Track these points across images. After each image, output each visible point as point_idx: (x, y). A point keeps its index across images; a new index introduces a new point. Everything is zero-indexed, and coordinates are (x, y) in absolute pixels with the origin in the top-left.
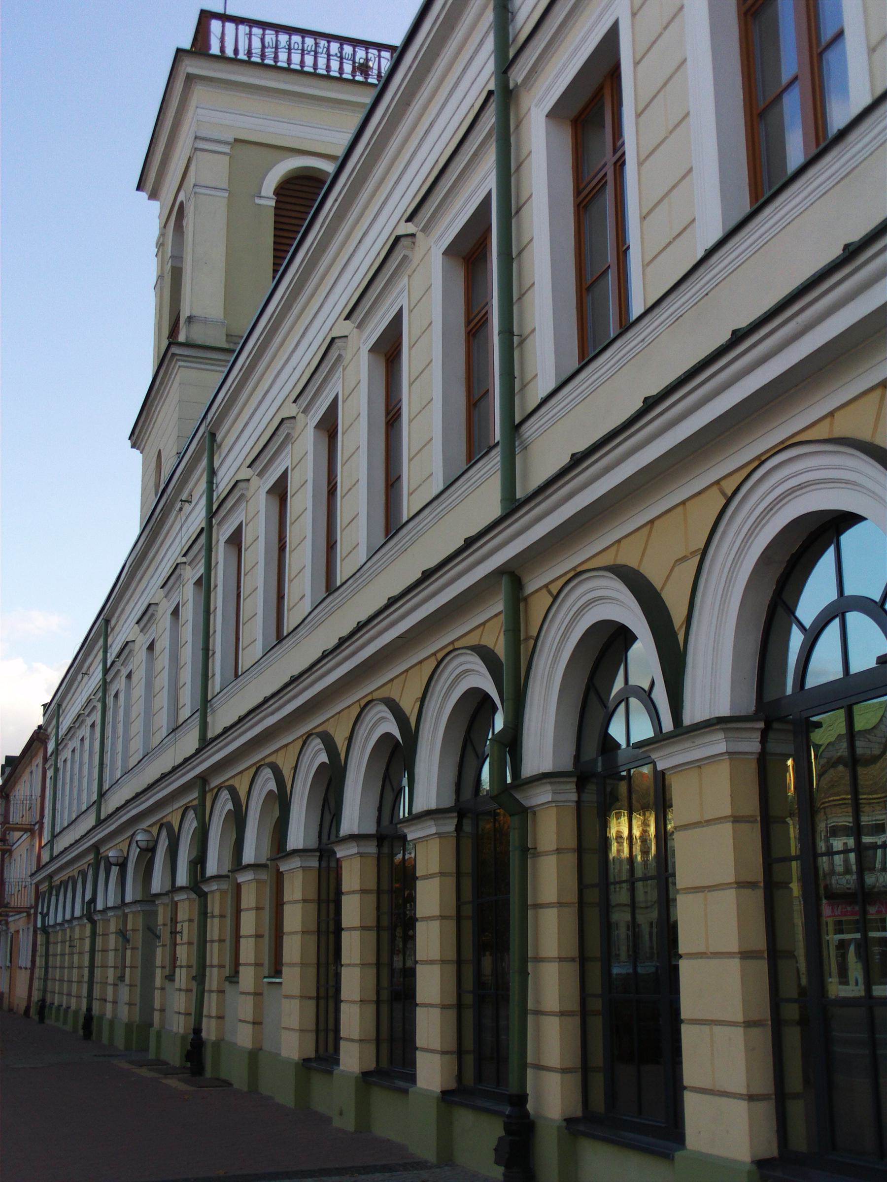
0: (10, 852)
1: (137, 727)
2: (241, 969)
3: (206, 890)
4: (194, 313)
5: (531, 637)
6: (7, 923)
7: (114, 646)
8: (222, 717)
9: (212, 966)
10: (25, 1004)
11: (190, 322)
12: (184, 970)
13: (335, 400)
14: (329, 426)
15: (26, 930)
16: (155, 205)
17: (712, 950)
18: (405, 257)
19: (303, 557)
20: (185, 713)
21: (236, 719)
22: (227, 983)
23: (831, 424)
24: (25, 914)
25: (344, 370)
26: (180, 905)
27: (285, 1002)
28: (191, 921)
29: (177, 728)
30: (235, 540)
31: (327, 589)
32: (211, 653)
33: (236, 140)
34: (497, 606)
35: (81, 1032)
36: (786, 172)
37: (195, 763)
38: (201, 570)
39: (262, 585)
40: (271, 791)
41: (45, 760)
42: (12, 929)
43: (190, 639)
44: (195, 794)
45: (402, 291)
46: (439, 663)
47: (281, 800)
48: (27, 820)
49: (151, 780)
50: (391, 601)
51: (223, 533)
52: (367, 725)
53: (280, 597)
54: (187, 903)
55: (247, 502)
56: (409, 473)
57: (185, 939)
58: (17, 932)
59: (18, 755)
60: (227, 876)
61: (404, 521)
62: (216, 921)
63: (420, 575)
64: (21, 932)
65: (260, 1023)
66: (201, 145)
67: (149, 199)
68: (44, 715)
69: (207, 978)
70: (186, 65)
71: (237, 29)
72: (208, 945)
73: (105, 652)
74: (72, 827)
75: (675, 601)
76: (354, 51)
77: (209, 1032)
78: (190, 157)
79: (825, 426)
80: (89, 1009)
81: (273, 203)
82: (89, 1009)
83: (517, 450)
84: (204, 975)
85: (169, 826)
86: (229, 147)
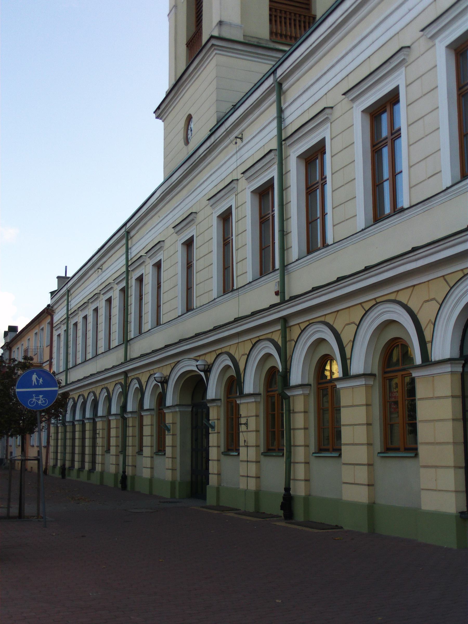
2: (144, 448)
3: (126, 416)
5: (293, 340)
8: (139, 347)
9: (129, 446)
12: (100, 448)
20: (114, 343)
22: (262, 456)
23: (397, 295)
26: (112, 422)
27: (111, 457)
28: (103, 429)
30: (140, 279)
31: (140, 333)
35: (120, 486)
38: (65, 328)
40: (137, 388)
43: (150, 291)
45: (161, 254)
47: (109, 399)
51: (135, 275)
52: (309, 333)
54: (101, 422)
55: (331, 123)
56: (238, 269)
57: (101, 436)
62: (131, 429)
65: (153, 468)
75: (346, 337)
77: (129, 471)
79: (394, 295)
80: (124, 472)
82: (124, 472)
84: (126, 450)
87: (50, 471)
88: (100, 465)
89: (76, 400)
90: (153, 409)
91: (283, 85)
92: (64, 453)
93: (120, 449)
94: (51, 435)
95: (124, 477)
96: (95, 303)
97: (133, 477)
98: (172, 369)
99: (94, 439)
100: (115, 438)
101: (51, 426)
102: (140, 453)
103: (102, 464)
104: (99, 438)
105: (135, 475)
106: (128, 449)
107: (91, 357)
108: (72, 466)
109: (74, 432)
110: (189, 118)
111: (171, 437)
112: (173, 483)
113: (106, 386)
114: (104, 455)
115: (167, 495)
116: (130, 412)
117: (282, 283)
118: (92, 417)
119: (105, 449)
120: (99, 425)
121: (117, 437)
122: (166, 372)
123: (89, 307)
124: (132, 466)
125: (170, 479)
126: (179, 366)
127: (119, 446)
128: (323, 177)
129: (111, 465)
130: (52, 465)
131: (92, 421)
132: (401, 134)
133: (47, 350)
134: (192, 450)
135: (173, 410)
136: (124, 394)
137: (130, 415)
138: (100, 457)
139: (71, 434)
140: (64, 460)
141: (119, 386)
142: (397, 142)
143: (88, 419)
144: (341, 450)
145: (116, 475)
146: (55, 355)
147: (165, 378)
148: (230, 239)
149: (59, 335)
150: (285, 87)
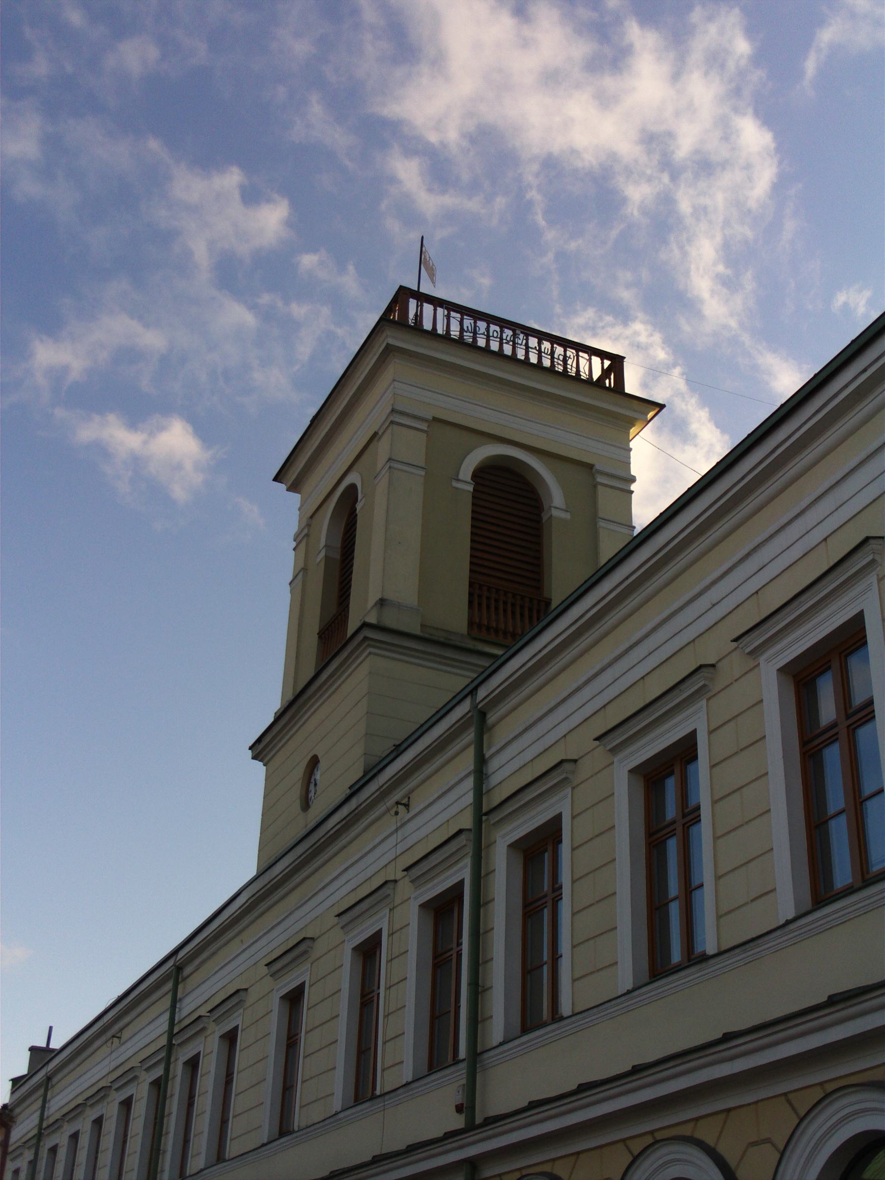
4: (385, 597)
7: (52, 1102)
11: (382, 605)
16: (295, 498)
33: (435, 419)
36: (819, 725)
37: (432, 1152)
51: (184, 1055)
63: (526, 1104)
66: (398, 419)
67: (287, 490)
70: (387, 336)
71: (435, 310)
76: (552, 347)
78: (376, 434)
81: (470, 488)
86: (426, 425)
91: (488, 716)
98: (635, 1159)
110: (314, 762)
117: (471, 1088)
123: (109, 1099)
128: (556, 886)
132: (874, 711)
142: (694, 830)
148: (375, 994)
150: (491, 719)
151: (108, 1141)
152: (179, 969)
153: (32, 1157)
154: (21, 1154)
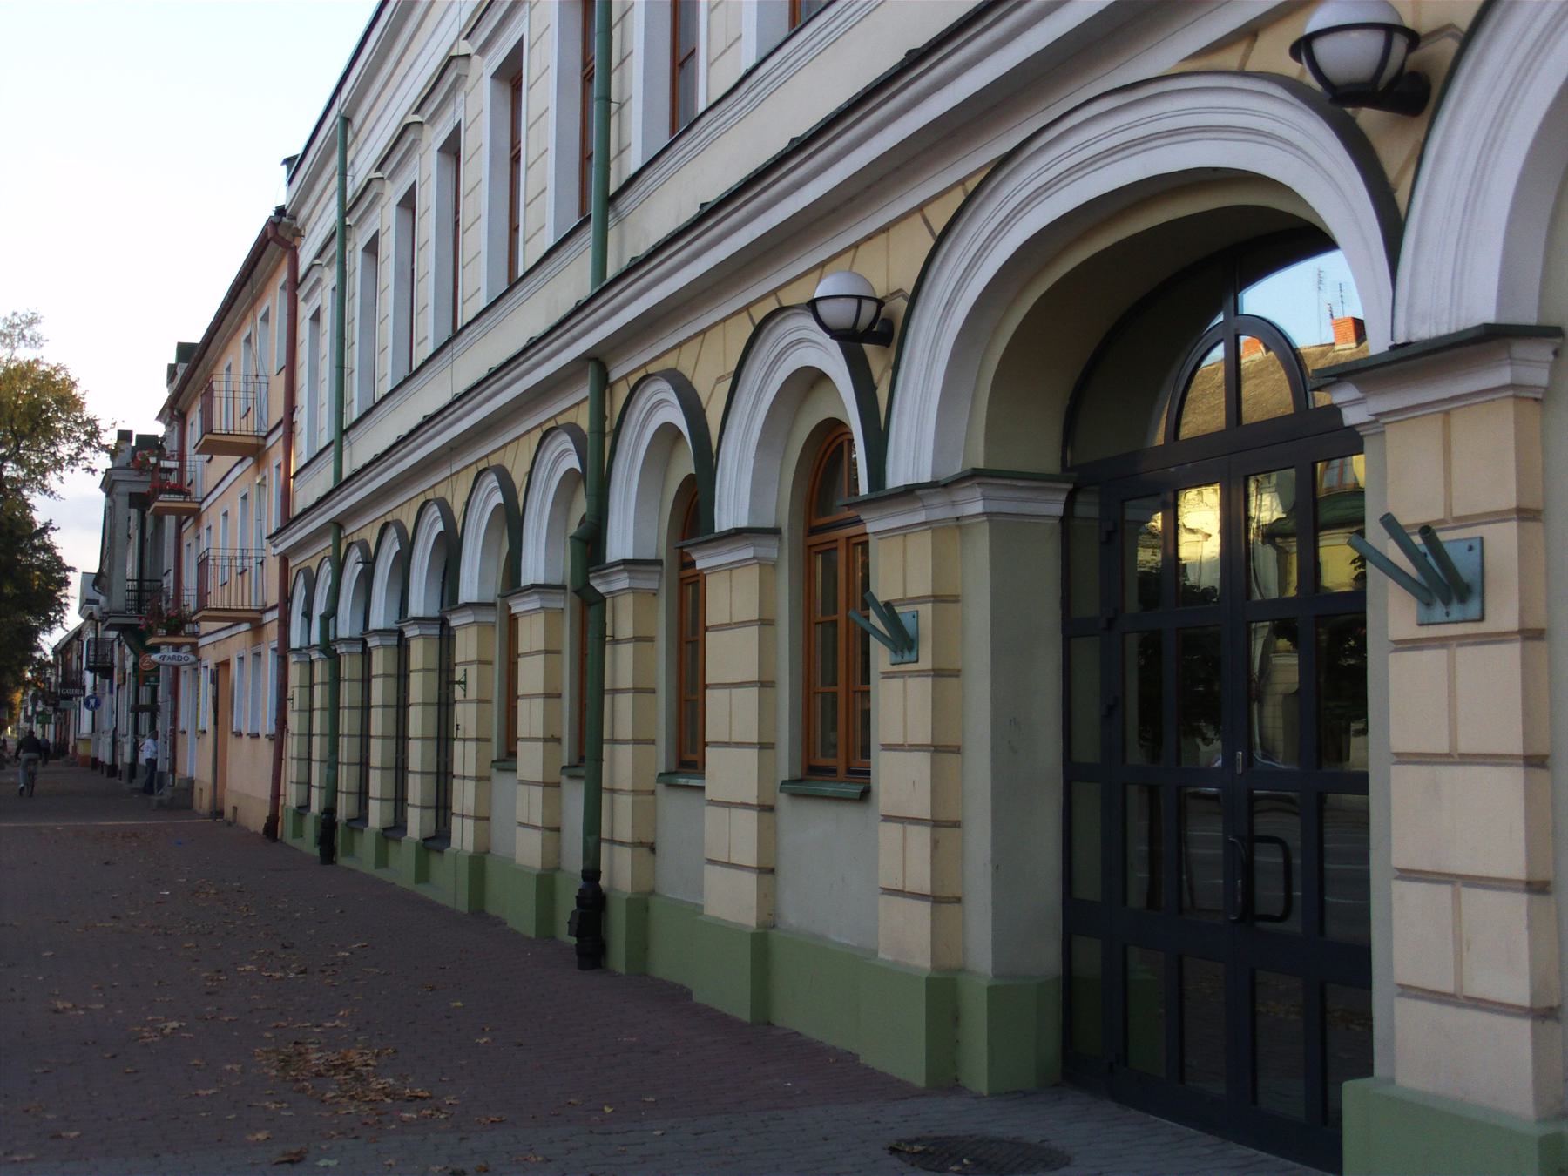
0: (196, 514)
1: (386, 333)
3: (601, 589)
6: (195, 649)
7: (358, 163)
9: (614, 741)
10: (265, 812)
12: (471, 746)
13: (519, 44)
14: (510, 75)
15: (249, 659)
17: (910, 741)
18: (414, 141)
19: (478, 241)
21: (420, 419)
24: (245, 626)
25: (531, 9)
26: (523, 625)
29: (376, 406)
32: (614, 107)
34: (584, 391)
39: (642, 46)
40: (572, 470)
41: (294, 284)
42: (210, 658)
44: (329, 542)
46: (970, 198)
47: (511, 518)
48: (248, 427)
49: (802, 125)
50: (706, 208)
51: (360, 239)
53: (514, 229)
54: (473, 631)
57: (473, 693)
58: (225, 664)
59: (198, 341)
60: (493, 605)
61: (700, 111)
64: (234, 664)
65: (772, 871)
68: (290, 182)
69: (605, 765)
72: (607, 699)
73: (343, 175)
74: (368, 421)
77: (620, 872)
80: (591, 874)
82: (591, 874)
83: (610, 224)
85: (400, 526)
87: (286, 827)
88: (469, 823)
89: (373, 547)
90: (775, 532)
92: (332, 763)
93: (565, 754)
94: (289, 695)
95: (593, 901)
96: (448, 113)
97: (641, 905)
98: (940, 240)
99: (444, 705)
100: (539, 703)
101: (293, 658)
102: (506, 765)
103: (476, 818)
104: (465, 701)
105: (653, 892)
106: (612, 752)
107: (389, 388)
108: (362, 817)
109: (402, 676)
111: (921, 688)
112: (943, 991)
113: (494, 460)
114: (488, 779)
115: (905, 1059)
116: (625, 562)
118: (434, 612)
119: (494, 751)
120: (467, 646)
121: (551, 695)
122: (889, 269)
123: (424, 145)
124: (635, 845)
125: (921, 960)
126: (1006, 190)
127: (559, 740)
129: (520, 830)
130: (294, 805)
131: (435, 631)
133: (279, 384)
134: (1073, 772)
135: (937, 509)
136: (595, 480)
137: (622, 581)
138: (470, 786)
139: (357, 686)
140: (332, 790)
141: (564, 442)
143: (418, 620)
144: (869, 773)
145: (546, 881)
146: (302, 398)
147: (880, 303)
149: (316, 317)
151: (479, 166)
152: (346, 121)
153: (334, 282)
154: (319, 281)
